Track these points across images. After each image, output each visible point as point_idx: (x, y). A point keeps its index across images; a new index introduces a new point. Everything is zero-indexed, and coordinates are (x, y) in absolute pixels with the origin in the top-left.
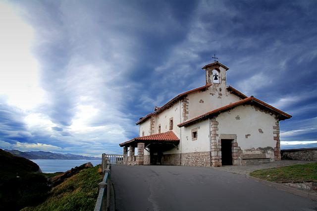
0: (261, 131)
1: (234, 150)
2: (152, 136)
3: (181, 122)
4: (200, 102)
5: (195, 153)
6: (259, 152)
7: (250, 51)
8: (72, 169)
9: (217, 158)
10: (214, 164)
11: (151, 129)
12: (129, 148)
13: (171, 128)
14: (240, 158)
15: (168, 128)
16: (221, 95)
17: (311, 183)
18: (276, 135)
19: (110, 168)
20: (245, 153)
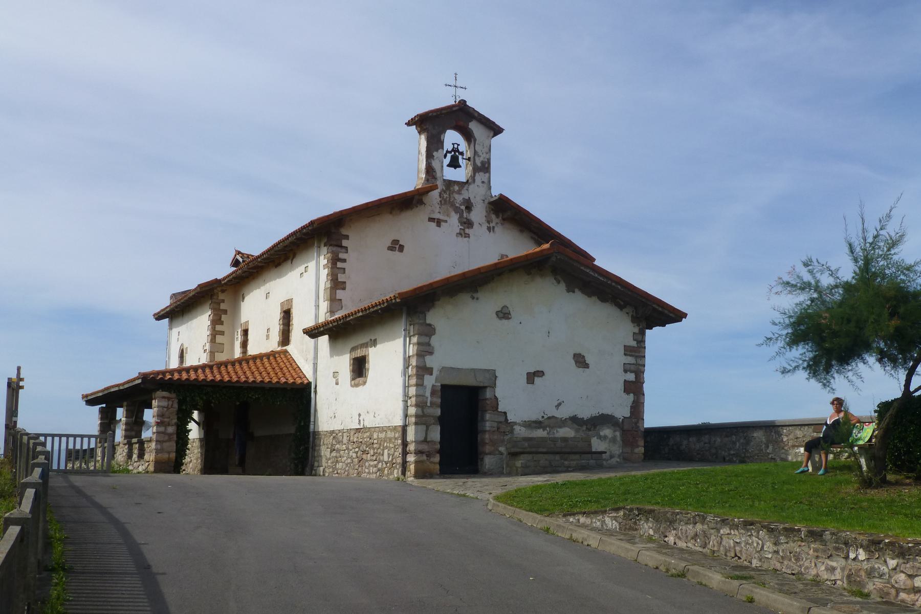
0: (580, 361)
1: (489, 422)
2: (219, 365)
3: (317, 316)
4: (391, 249)
5: (358, 430)
6: (566, 432)
7: (158, 373)
8: (594, 260)
9: (425, 447)
10: (412, 467)
11: (213, 339)
12: (120, 413)
13: (285, 339)
14: (502, 449)
15: (276, 337)
16: (468, 224)
17: (621, 513)
18: (631, 377)
19: (44, 476)
20: (520, 432)
